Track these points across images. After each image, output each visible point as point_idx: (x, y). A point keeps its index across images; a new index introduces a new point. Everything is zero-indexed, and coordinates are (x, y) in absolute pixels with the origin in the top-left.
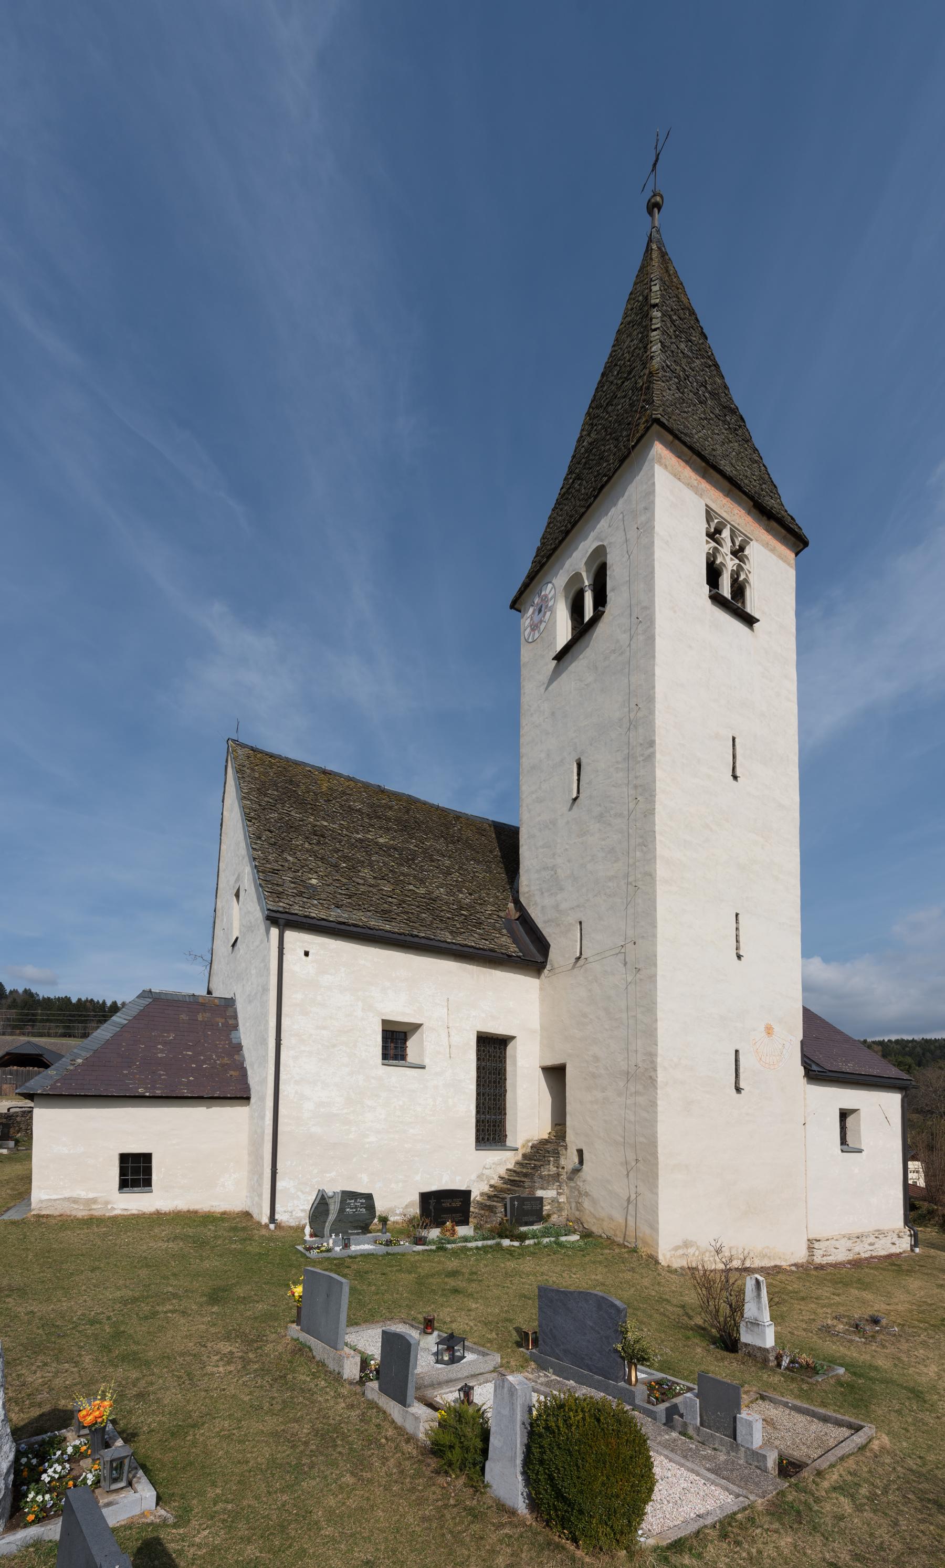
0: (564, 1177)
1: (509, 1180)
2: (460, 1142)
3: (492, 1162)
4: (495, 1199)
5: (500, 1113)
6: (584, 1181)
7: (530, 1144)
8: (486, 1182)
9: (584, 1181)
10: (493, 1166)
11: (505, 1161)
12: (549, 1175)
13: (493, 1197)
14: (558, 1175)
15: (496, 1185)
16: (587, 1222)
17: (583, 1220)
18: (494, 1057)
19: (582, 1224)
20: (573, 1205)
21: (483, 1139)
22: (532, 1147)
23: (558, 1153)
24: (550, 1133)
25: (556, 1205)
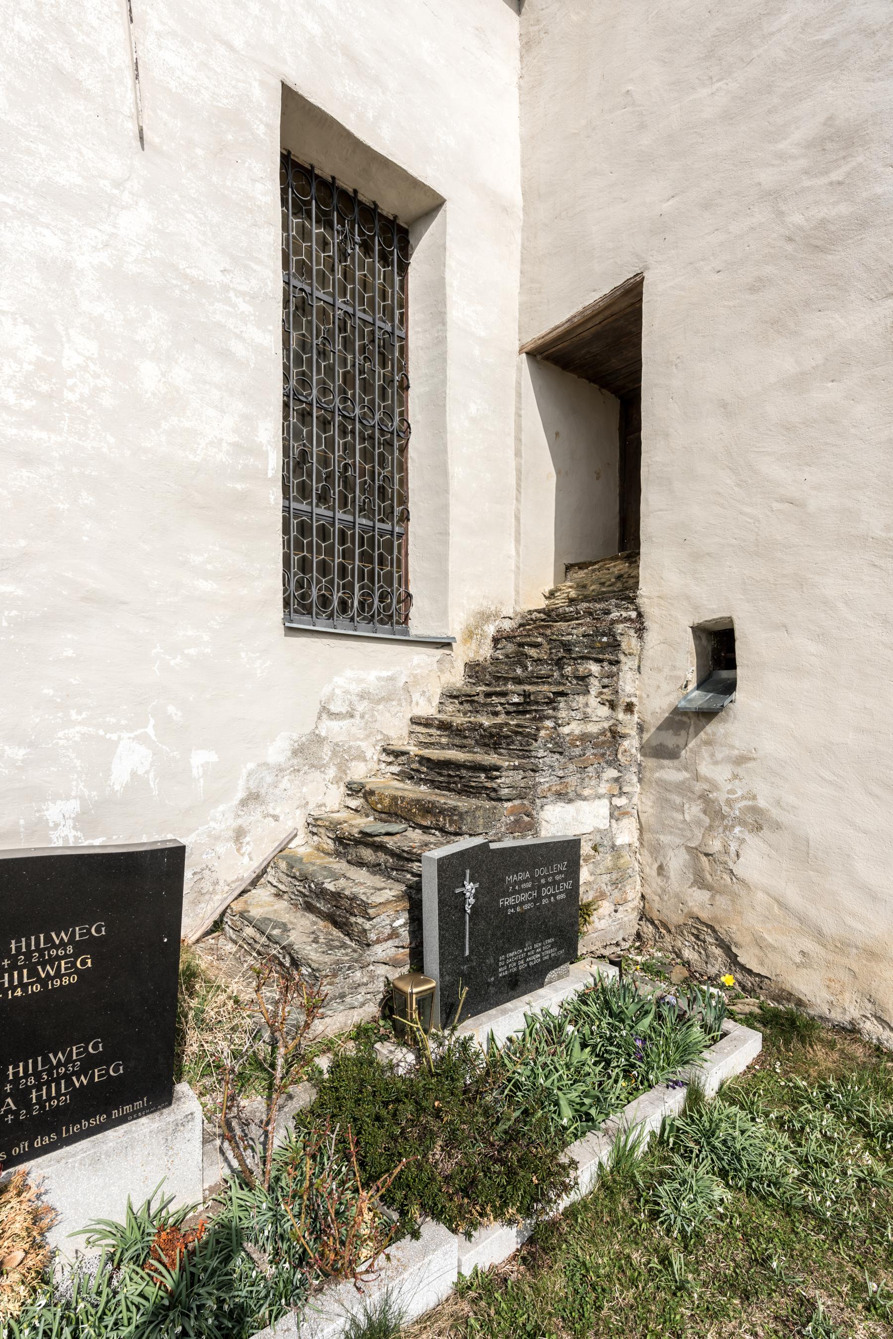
0: (631, 744)
1: (424, 760)
2: (206, 586)
3: (355, 688)
4: (367, 854)
5: (388, 515)
6: (741, 760)
7: (491, 630)
8: (332, 772)
9: (741, 760)
10: (362, 707)
11: (406, 689)
12: (584, 737)
13: (357, 842)
14: (615, 735)
15: (372, 783)
16: (759, 943)
17: (733, 929)
18: (365, 285)
19: (726, 948)
20: (677, 861)
21: (325, 602)
22: (496, 641)
23: (615, 646)
24: (552, 595)
25: (608, 861)
